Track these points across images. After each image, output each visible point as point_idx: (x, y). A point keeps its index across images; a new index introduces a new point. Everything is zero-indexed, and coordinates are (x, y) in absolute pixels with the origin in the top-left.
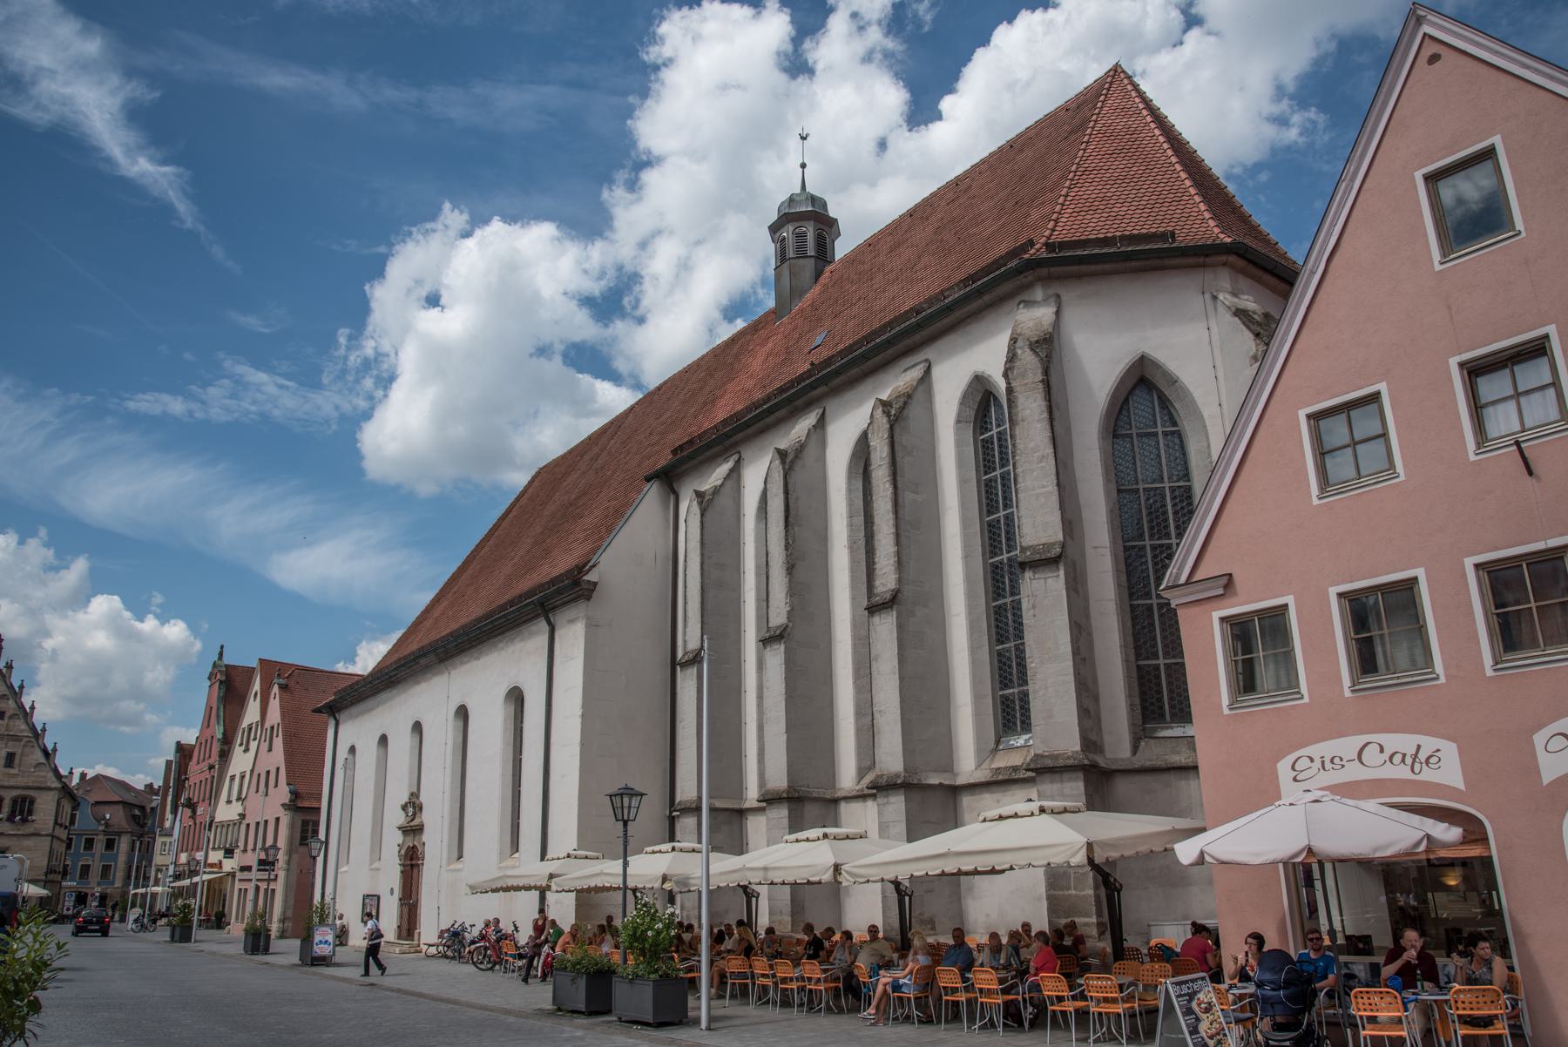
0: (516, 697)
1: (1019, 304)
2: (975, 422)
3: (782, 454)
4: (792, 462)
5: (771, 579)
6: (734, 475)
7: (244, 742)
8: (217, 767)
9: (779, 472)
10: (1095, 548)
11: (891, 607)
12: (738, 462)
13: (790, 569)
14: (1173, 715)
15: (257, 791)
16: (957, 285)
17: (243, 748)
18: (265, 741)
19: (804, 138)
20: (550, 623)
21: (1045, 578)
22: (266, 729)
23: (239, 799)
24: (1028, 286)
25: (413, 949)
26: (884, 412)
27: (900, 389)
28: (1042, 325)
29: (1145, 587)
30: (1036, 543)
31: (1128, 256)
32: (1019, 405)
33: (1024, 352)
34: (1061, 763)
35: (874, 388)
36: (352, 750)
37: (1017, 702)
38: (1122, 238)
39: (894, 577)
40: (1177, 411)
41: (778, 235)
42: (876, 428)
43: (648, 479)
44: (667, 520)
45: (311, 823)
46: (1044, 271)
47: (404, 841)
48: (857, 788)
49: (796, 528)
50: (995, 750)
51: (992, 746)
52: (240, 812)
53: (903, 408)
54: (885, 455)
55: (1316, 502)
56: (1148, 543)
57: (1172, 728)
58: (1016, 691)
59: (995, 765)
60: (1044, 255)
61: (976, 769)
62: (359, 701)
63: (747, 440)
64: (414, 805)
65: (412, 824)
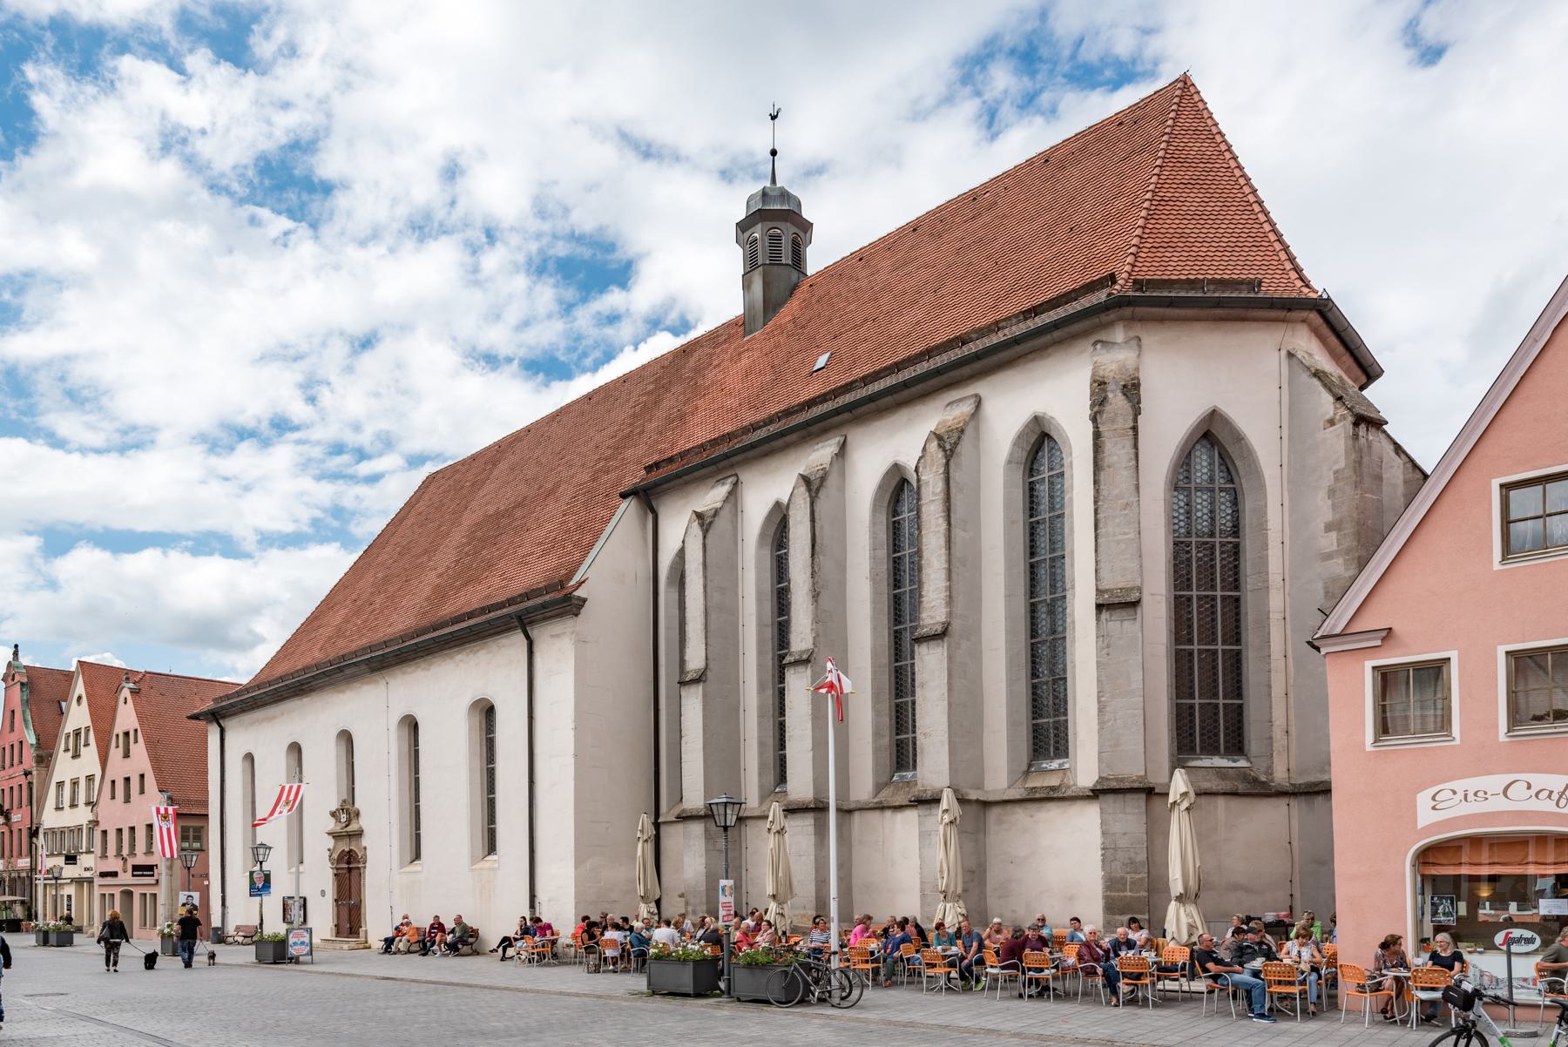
0: (487, 712)
1: (1095, 344)
2: (1025, 464)
3: (806, 480)
4: (818, 490)
6: (732, 498)
7: (71, 747)
8: (34, 773)
10: (1152, 595)
11: (942, 639)
12: (736, 484)
13: (816, 595)
14: (1202, 749)
15: (113, 797)
16: (1016, 316)
17: (70, 754)
18: (117, 747)
19: (773, 118)
20: (528, 637)
21: (1122, 621)
22: (117, 736)
23: (88, 804)
24: (1110, 325)
25: (361, 946)
26: (939, 446)
27: (950, 424)
28: (1127, 370)
29: (1189, 634)
30: (1112, 586)
31: (1219, 303)
32: (1106, 450)
33: (1115, 396)
34: (1127, 785)
35: (909, 419)
36: (249, 758)
37: (1051, 731)
38: (1213, 281)
39: (944, 610)
40: (1237, 471)
41: (747, 234)
42: (929, 461)
43: (624, 496)
44: (645, 540)
45: (191, 830)
46: (1128, 311)
47: (334, 847)
48: (875, 800)
49: (821, 557)
50: (1027, 773)
51: (1025, 767)
52: (91, 819)
53: (956, 444)
54: (939, 490)
55: (1497, 566)
56: (1219, 593)
57: (1201, 759)
58: (1051, 720)
59: (1030, 785)
60: (1131, 293)
61: (1009, 787)
62: (253, 709)
63: (747, 462)
64: (347, 810)
65: (348, 829)
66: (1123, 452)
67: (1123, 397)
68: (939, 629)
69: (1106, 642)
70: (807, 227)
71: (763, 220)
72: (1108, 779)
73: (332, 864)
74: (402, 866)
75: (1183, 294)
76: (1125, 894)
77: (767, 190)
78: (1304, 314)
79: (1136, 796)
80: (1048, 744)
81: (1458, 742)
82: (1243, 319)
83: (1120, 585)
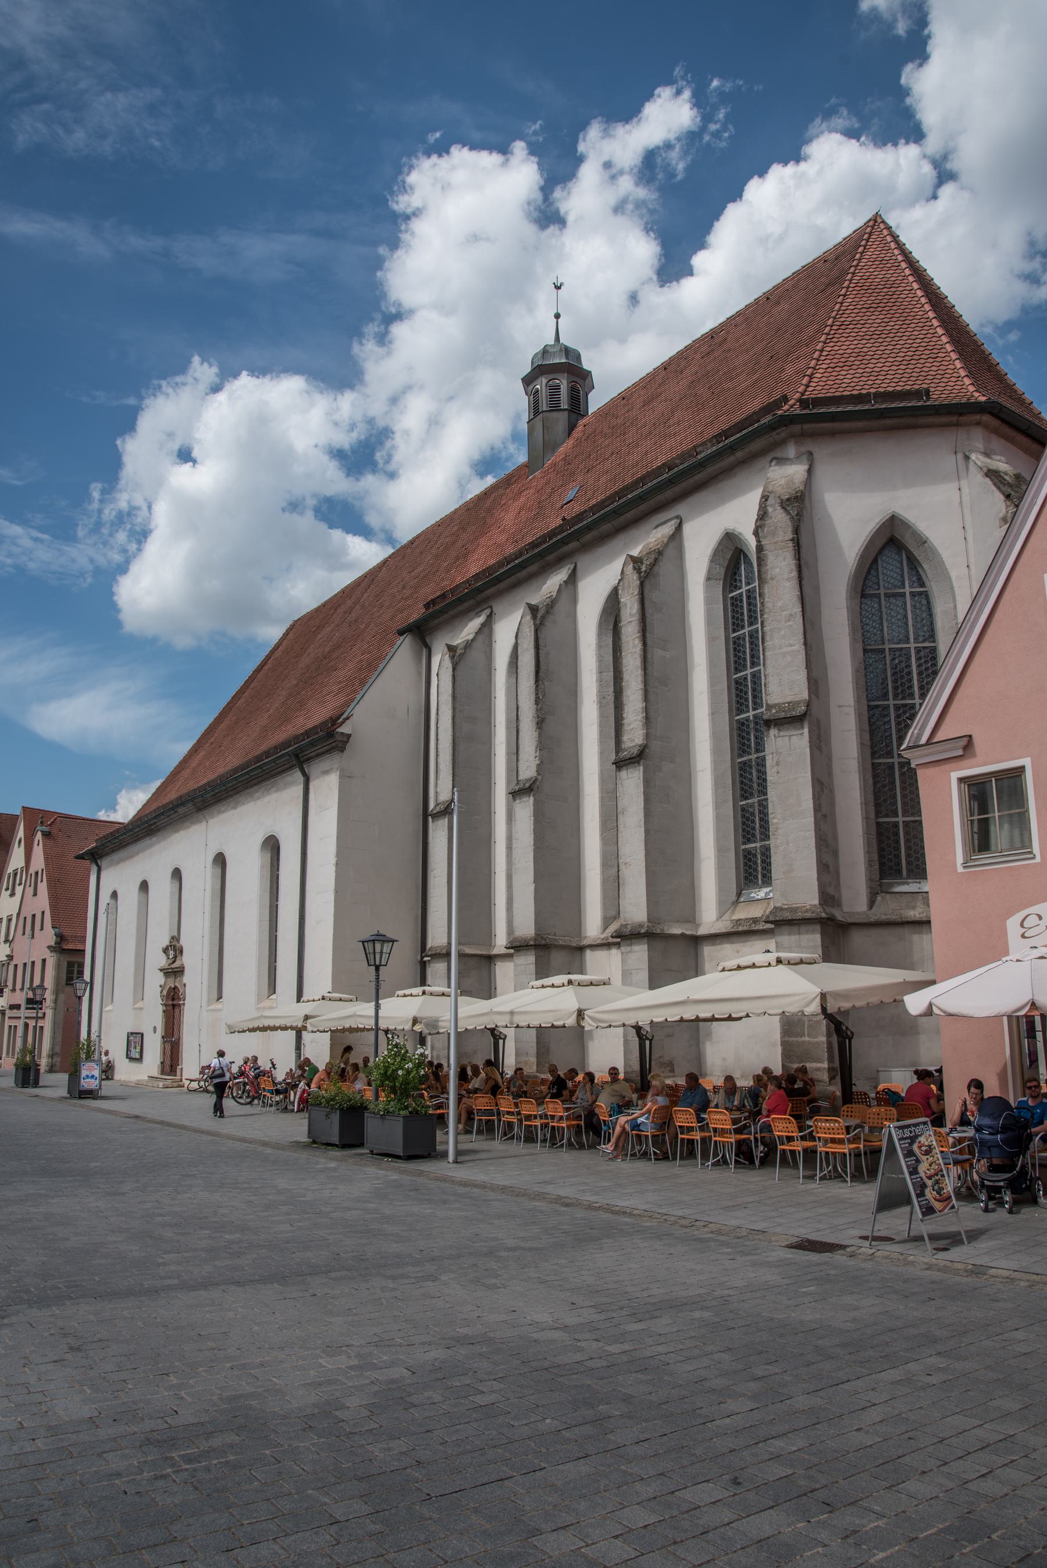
0: (272, 846)
1: (771, 461)
3: (533, 609)
4: (543, 617)
5: (521, 734)
6: (486, 630)
9: (530, 627)
10: (840, 706)
11: (638, 762)
12: (490, 617)
13: (540, 723)
15: (24, 934)
17: (9, 892)
20: (304, 774)
21: (790, 736)
24: (782, 443)
26: (634, 568)
27: (651, 546)
30: (781, 701)
31: (881, 414)
34: (799, 915)
36: (114, 895)
37: (759, 856)
39: (642, 732)
41: (531, 387)
42: (626, 584)
43: (401, 633)
44: (420, 673)
45: (76, 966)
46: (796, 428)
49: (546, 683)
50: (736, 902)
51: (734, 898)
54: (635, 611)
56: (891, 702)
57: (908, 883)
58: (758, 845)
59: (736, 917)
60: (798, 412)
61: (717, 920)
64: (174, 949)
65: (173, 966)
66: (783, 563)
67: (782, 511)
68: (635, 751)
69: (775, 760)
70: (586, 375)
71: (542, 374)
72: (782, 909)
73: (162, 1000)
74: (209, 1003)
75: (850, 408)
76: (803, 1039)
77: (548, 348)
78: (977, 417)
79: (810, 928)
80: (756, 870)
81: (1038, 859)
82: (915, 427)
83: (789, 699)
